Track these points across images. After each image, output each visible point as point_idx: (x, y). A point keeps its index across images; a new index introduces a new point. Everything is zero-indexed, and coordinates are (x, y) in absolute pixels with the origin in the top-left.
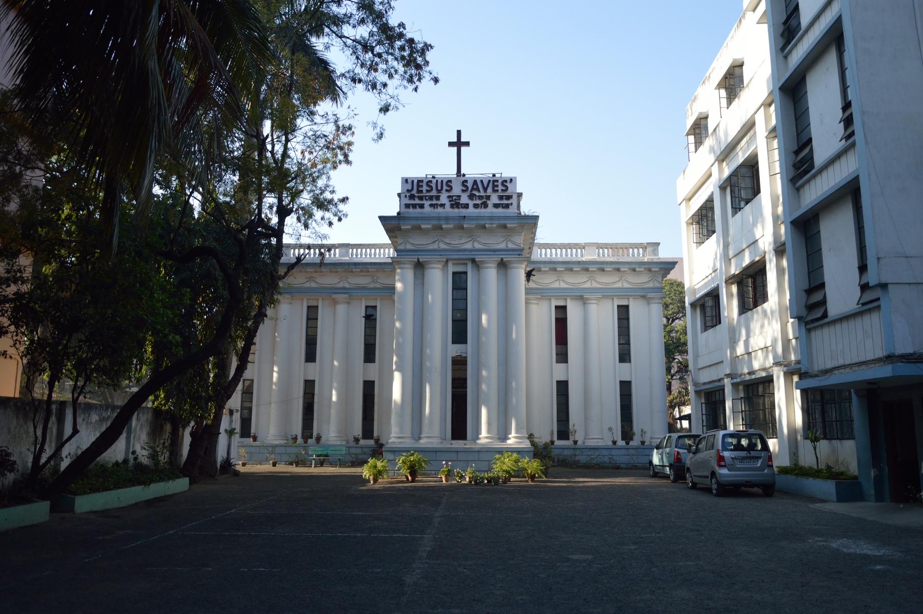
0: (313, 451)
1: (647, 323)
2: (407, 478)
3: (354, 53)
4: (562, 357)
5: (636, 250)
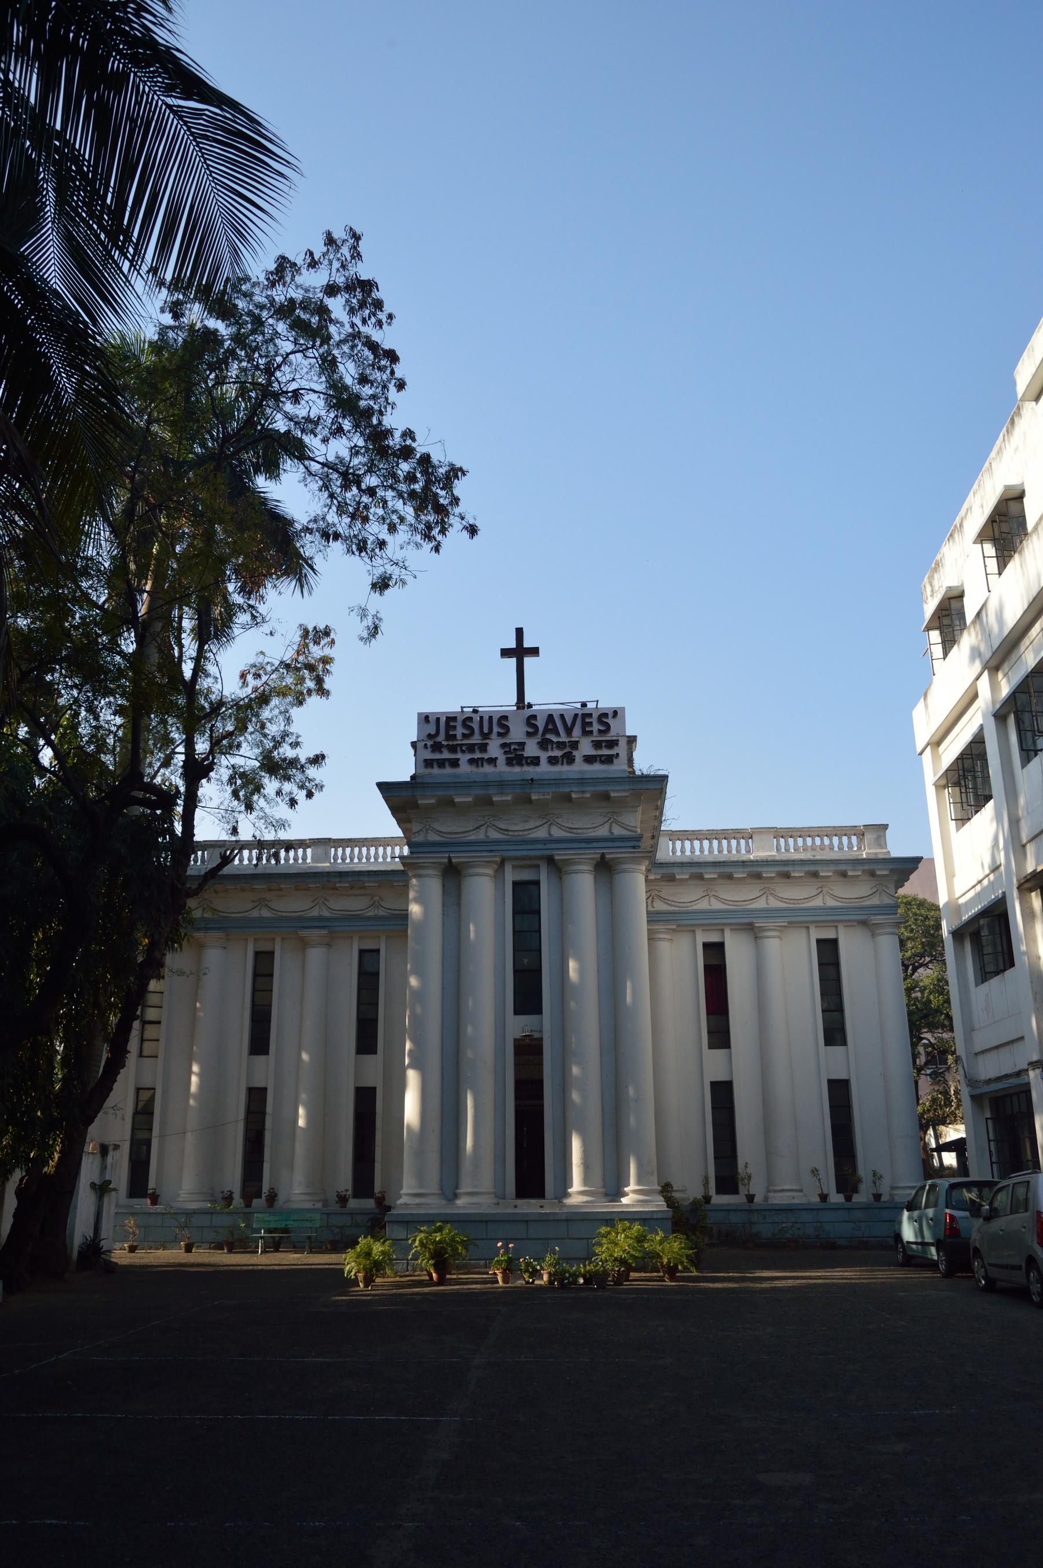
0: (262, 1222)
1: (872, 968)
2: (430, 1275)
3: (327, 488)
4: (719, 1035)
5: (845, 839)
